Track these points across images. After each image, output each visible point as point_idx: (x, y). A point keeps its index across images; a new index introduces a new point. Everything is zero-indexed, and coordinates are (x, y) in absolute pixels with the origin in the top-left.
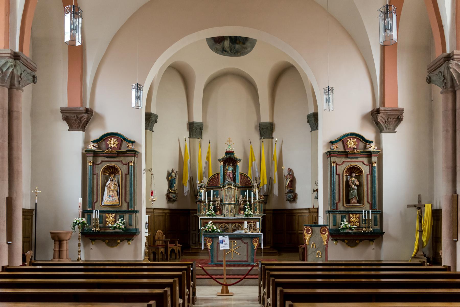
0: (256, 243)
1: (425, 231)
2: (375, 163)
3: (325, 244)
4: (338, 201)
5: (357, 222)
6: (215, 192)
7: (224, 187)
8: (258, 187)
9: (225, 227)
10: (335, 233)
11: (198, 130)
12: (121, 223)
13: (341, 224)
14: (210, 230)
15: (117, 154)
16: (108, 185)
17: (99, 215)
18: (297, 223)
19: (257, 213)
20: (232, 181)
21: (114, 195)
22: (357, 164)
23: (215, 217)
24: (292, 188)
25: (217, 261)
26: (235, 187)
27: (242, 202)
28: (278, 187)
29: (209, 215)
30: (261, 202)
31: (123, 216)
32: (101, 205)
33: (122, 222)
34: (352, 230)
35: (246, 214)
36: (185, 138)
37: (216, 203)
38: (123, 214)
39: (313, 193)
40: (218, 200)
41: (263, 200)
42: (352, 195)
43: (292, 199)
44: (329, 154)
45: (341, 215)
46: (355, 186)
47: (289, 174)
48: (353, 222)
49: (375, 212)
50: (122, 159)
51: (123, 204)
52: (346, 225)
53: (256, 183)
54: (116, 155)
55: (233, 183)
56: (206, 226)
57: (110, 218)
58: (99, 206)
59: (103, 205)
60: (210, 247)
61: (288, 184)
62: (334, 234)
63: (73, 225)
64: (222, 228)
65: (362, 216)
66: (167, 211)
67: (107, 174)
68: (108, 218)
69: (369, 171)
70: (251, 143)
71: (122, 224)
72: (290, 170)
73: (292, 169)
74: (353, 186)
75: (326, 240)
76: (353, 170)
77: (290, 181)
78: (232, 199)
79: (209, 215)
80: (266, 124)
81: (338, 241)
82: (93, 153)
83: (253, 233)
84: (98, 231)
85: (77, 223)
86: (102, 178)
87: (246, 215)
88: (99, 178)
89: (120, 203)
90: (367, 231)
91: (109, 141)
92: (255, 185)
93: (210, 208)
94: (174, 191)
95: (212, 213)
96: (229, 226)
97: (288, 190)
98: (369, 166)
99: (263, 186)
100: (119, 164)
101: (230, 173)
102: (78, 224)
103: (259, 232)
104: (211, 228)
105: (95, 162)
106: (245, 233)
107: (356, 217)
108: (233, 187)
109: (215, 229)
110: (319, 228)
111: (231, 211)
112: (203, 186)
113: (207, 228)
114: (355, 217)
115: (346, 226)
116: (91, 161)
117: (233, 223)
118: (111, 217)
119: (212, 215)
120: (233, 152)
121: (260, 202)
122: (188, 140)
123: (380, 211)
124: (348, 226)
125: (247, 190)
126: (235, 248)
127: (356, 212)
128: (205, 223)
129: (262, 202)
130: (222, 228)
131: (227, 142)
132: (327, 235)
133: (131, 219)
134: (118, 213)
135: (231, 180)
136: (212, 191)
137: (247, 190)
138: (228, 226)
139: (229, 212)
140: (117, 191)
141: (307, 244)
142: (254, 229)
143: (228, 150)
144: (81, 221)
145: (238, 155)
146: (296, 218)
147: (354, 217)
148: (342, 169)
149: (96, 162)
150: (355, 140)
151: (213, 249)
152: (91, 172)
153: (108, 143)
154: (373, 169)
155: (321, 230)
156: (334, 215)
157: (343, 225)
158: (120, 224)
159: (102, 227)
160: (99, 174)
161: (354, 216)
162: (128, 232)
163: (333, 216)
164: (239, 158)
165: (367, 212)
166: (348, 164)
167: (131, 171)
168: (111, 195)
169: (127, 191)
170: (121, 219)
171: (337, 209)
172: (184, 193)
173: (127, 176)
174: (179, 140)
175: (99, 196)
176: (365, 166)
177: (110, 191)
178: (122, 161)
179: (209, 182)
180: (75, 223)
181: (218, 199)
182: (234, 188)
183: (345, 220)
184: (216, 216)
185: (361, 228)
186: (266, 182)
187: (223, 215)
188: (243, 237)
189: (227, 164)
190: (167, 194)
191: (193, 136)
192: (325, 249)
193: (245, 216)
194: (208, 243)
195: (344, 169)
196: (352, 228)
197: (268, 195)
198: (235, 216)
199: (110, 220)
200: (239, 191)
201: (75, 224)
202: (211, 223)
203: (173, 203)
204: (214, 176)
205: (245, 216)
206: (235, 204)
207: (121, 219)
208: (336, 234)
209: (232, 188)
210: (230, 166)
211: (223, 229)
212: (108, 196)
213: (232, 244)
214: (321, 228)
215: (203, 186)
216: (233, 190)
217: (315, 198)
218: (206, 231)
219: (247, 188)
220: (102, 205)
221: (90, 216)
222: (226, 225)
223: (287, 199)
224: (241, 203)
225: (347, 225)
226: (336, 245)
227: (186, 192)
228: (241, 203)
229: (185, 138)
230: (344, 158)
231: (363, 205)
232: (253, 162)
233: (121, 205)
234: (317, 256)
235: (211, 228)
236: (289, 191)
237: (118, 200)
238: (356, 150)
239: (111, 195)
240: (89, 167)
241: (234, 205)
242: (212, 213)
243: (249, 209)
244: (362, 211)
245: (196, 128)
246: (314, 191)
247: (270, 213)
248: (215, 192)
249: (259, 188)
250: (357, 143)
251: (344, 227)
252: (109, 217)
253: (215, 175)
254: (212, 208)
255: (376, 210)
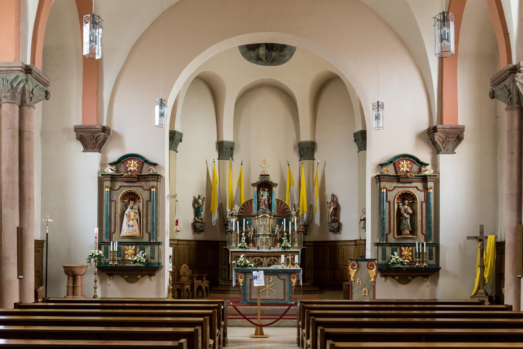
0: (294, 280)
1: (487, 266)
2: (431, 188)
3: (373, 280)
4: (388, 232)
5: (409, 255)
6: (248, 222)
7: (258, 216)
8: (297, 215)
9: (259, 262)
10: (383, 268)
11: (229, 150)
12: (142, 256)
13: (391, 258)
14: (242, 264)
15: (138, 178)
16: (128, 214)
17: (118, 247)
18: (341, 256)
19: (295, 246)
20: (267, 209)
21: (134, 224)
22: (410, 190)
23: (248, 250)
24: (336, 217)
25: (250, 300)
26: (270, 215)
27: (278, 233)
28: (320, 215)
29: (241, 247)
30: (299, 233)
31: (145, 248)
32: (120, 235)
33: (143, 255)
34: (404, 265)
35: (283, 246)
36: (214, 160)
37: (248, 234)
38: (144, 246)
39: (360, 223)
40: (251, 231)
41: (303, 230)
42: (404, 225)
43: (336, 230)
44: (379, 178)
45: (392, 248)
46: (408, 215)
47: (333, 201)
48: (405, 256)
49: (431, 245)
50: (142, 184)
51: (144, 235)
52: (396, 259)
53: (295, 211)
54: (137, 179)
55: (268, 211)
56: (238, 260)
57: (130, 250)
58: (117, 237)
59: (122, 236)
60: (242, 284)
61: (331, 212)
62: (383, 270)
63: (88, 258)
64: (255, 262)
65: (415, 248)
66: (192, 243)
67: (126, 201)
68: (404, 252)
69: (424, 197)
70: (289, 165)
71: (144, 257)
72: (334, 196)
73: (336, 195)
74: (406, 214)
75: (374, 276)
76: (406, 197)
77: (333, 209)
78: (267, 230)
79: (241, 247)
80: (306, 143)
81: (388, 277)
82: (110, 177)
83: (291, 268)
84: (116, 265)
85: (93, 256)
86: (121, 205)
87: (283, 247)
88: (117, 205)
89: (140, 234)
90: (421, 266)
91: (128, 163)
92: (294, 213)
93: (242, 240)
94: (201, 219)
95: (244, 245)
96: (263, 260)
97: (331, 219)
98: (423, 192)
99: (303, 215)
100: (139, 189)
101: (265, 199)
102: (94, 257)
103: (298, 266)
104: (244, 262)
105: (112, 187)
106: (282, 268)
107: (409, 250)
108: (268, 216)
109: (248, 264)
110: (366, 263)
111: (265, 243)
112: (234, 215)
113: (239, 263)
114: (408, 250)
115: (397, 261)
116: (108, 186)
117: (268, 257)
118: (130, 250)
119: (244, 247)
120: (268, 175)
121: (298, 233)
122: (217, 161)
123: (436, 244)
124: (400, 260)
125: (285, 219)
126: (270, 284)
127: (409, 245)
128: (236, 256)
129: (301, 233)
130: (255, 262)
131: (262, 164)
132: (375, 271)
133: (153, 251)
134: (138, 245)
135: (266, 208)
136: (244, 220)
137: (285, 219)
138: (262, 260)
139: (263, 244)
140: (137, 220)
141: (352, 280)
142: (292, 264)
143: (262, 173)
144: (97, 254)
145: (274, 179)
146: (340, 250)
147: (406, 250)
148: (392, 196)
149: (114, 187)
150: (409, 162)
151: (246, 286)
152: (108, 198)
153: (127, 165)
154: (428, 195)
155: (368, 265)
156: (383, 248)
157: (394, 259)
158: (141, 258)
159: (121, 261)
160: (117, 201)
161: (406, 249)
162: (150, 266)
163: (382, 249)
164: (275, 183)
165: (421, 244)
166: (401, 189)
167: (153, 197)
168: (131, 225)
169: (149, 220)
170: (142, 252)
171: (387, 241)
172: (212, 222)
173: (149, 203)
174: (206, 162)
175: (117, 226)
176: (419, 192)
177: (129, 220)
178: (143, 186)
179: (240, 210)
180: (90, 256)
181: (251, 229)
182: (270, 217)
183: (396, 253)
184: (248, 249)
185: (414, 263)
186: (306, 210)
187: (256, 248)
188: (279, 272)
189: (261, 189)
190: (193, 223)
191: (222, 157)
192: (372, 286)
193: (282, 249)
194: (240, 279)
195: (395, 195)
196: (404, 263)
197: (309, 224)
198: (270, 249)
199: (130, 253)
200: (275, 220)
201: (90, 257)
202: (244, 257)
203: (199, 234)
204: (247, 203)
205: (282, 249)
206: (270, 236)
207: (142, 252)
208: (385, 270)
209: (267, 217)
210: (265, 191)
211: (257, 263)
212: (128, 226)
213: (267, 281)
214: (369, 263)
215: (234, 215)
216: (268, 219)
217: (362, 228)
218: (238, 266)
219: (285, 217)
220: (121, 235)
221: (108, 248)
222: (260, 258)
223: (330, 229)
224: (277, 233)
225: (398, 259)
226: (385, 281)
227: (214, 222)
228: (277, 233)
229: (214, 160)
230: (395, 183)
231: (417, 236)
232: (292, 187)
233: (141, 236)
234: (363, 295)
235: (244, 262)
236: (332, 220)
237: (138, 230)
238: (409, 174)
239: (131, 225)
240: (106, 193)
241: (270, 236)
242: (244, 245)
243: (287, 240)
244: (416, 244)
245: (226, 148)
246: (361, 220)
247: (311, 246)
248: (248, 222)
249: (297, 216)
250: (410, 166)
251: (395, 261)
252: (129, 249)
253: (248, 202)
254: (244, 240)
255: (431, 242)
